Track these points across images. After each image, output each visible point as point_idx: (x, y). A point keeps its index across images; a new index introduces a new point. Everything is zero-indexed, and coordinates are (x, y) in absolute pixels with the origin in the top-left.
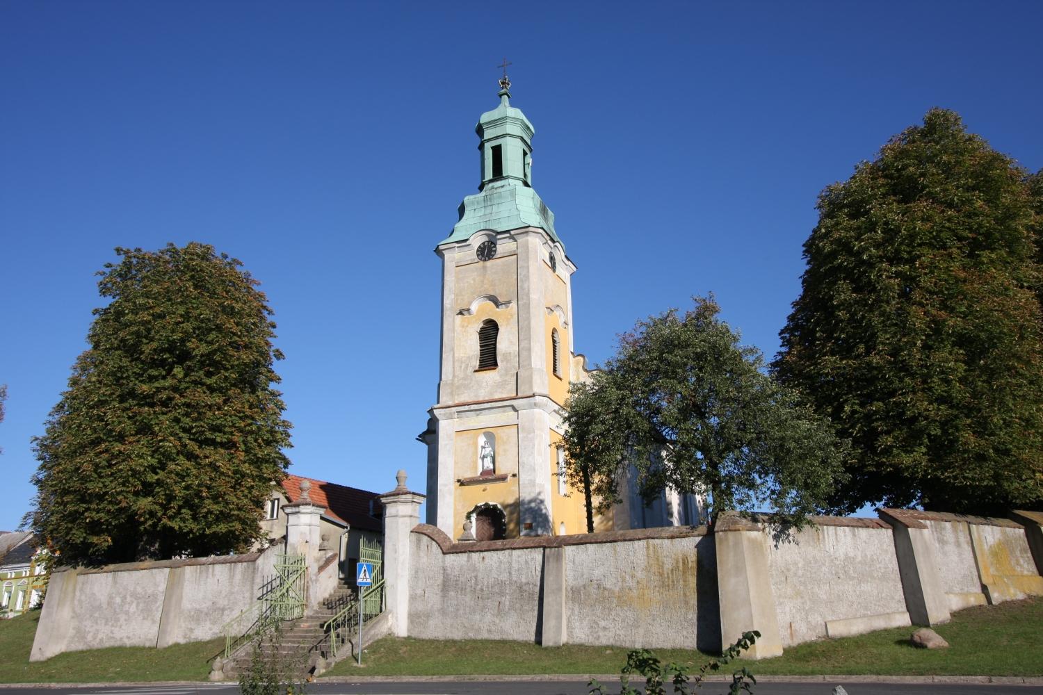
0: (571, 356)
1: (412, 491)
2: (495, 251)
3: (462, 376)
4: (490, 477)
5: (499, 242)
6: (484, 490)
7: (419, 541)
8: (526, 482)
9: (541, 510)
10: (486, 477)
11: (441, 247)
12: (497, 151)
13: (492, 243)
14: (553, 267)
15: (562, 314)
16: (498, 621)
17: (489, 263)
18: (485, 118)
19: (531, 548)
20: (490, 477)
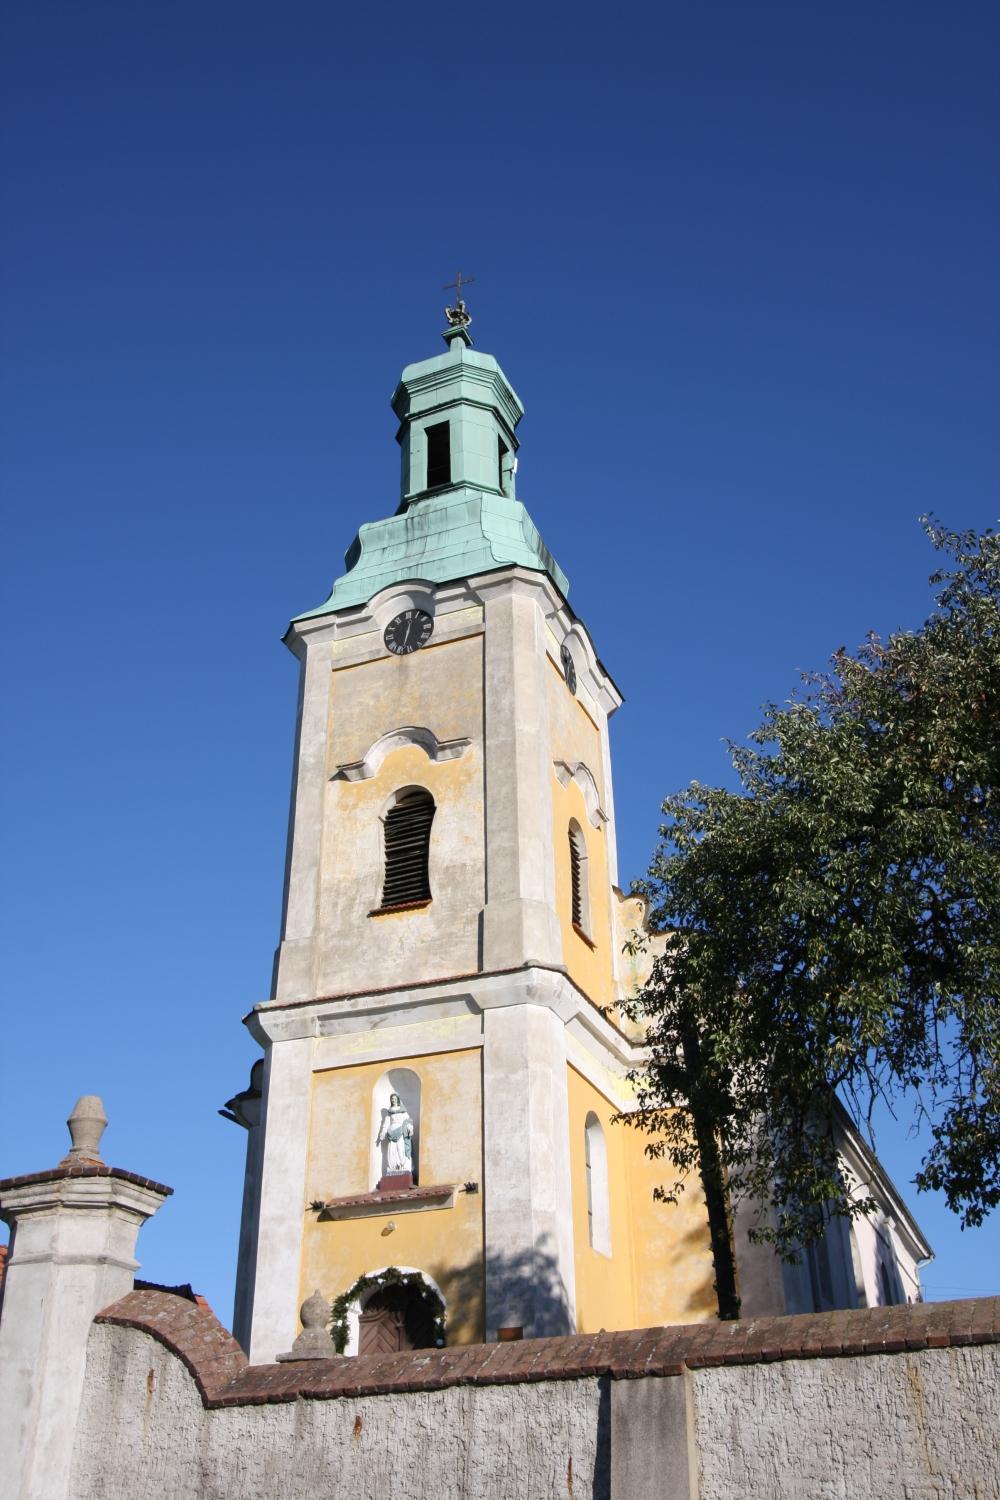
0: (614, 897)
1: (110, 1165)
2: (430, 631)
3: (336, 927)
4: (404, 1193)
5: (439, 609)
6: (386, 1232)
7: (120, 1354)
8: (505, 1207)
9: (549, 1289)
10: (393, 1194)
11: (298, 627)
12: (439, 438)
13: (423, 613)
14: (570, 679)
15: (592, 790)
17: (414, 658)
18: (410, 373)
19: (552, 1377)
20: (404, 1193)
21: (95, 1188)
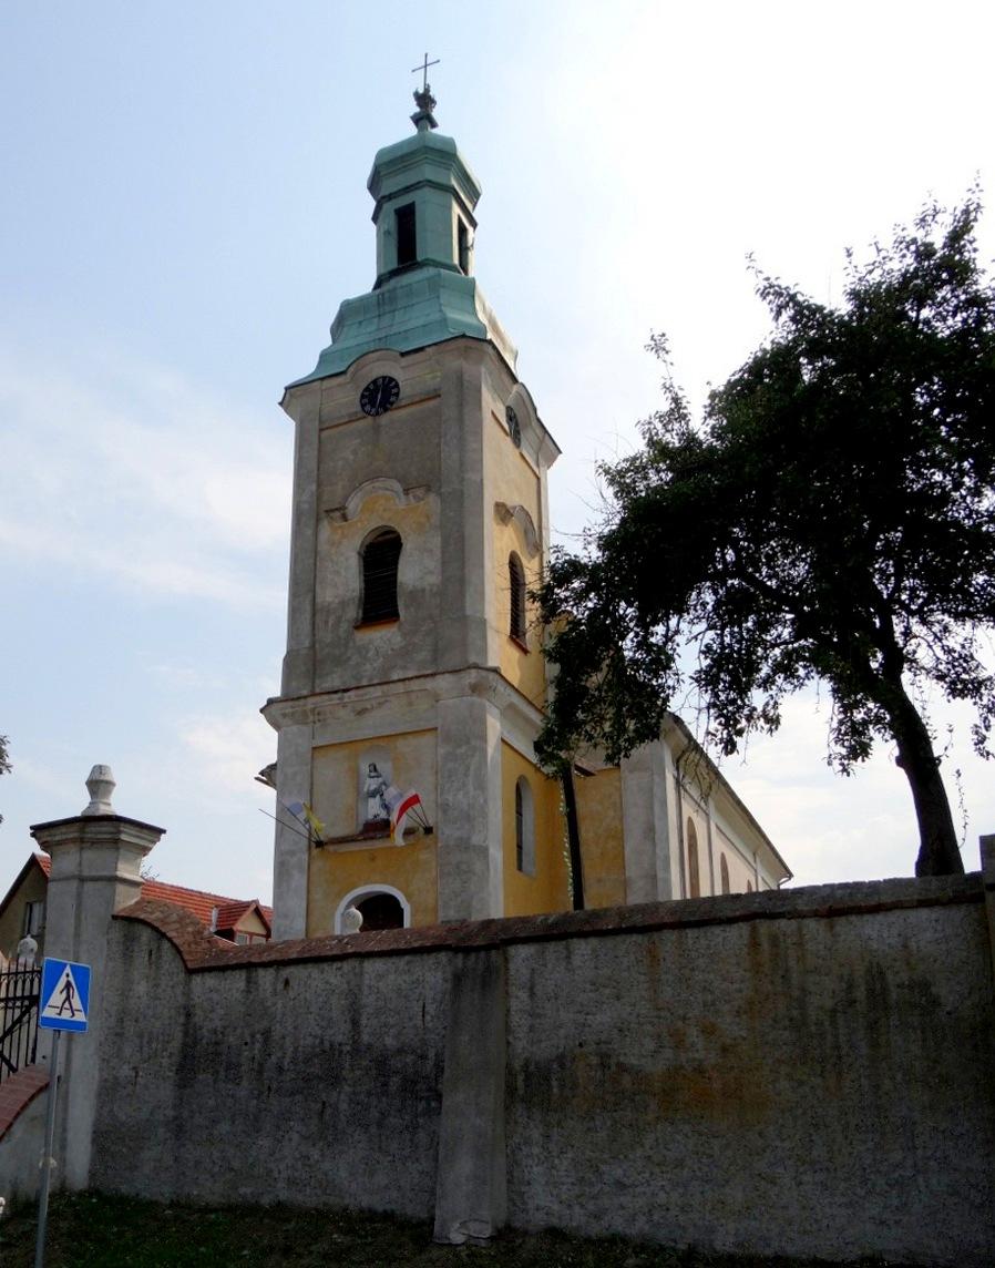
2: (397, 394)
16: (315, 1154)
17: (385, 419)
21: (104, 829)
